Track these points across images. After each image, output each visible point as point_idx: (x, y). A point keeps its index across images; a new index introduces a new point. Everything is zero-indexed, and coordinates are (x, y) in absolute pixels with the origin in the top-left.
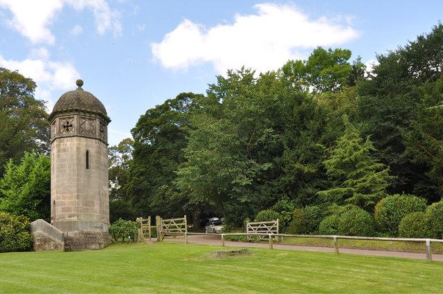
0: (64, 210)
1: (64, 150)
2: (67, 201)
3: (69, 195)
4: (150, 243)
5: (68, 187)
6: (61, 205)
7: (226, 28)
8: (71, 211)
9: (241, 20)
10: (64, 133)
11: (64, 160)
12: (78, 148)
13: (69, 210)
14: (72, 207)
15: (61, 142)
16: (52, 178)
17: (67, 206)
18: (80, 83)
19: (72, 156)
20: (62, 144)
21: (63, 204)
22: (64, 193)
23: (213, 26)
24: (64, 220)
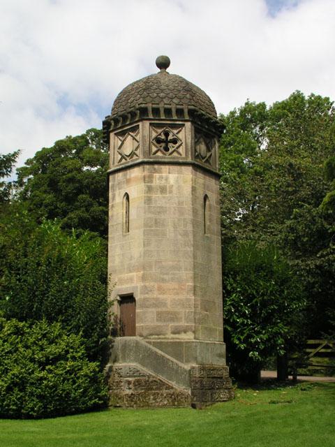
0: (160, 316)
1: (163, 190)
2: (168, 298)
3: (174, 285)
4: (11, 181)
5: (173, 268)
6: (155, 305)
7: (46, 147)
8: (178, 320)
9: (40, 150)
10: (159, 154)
11: (162, 210)
12: (194, 189)
13: (173, 317)
14: (183, 311)
15: (156, 171)
16: (222, 300)
17: (170, 308)
18: (163, 64)
19: (180, 203)
20: (157, 175)
21: (158, 303)
22: (163, 280)
23: (62, 141)
24: (161, 338)
